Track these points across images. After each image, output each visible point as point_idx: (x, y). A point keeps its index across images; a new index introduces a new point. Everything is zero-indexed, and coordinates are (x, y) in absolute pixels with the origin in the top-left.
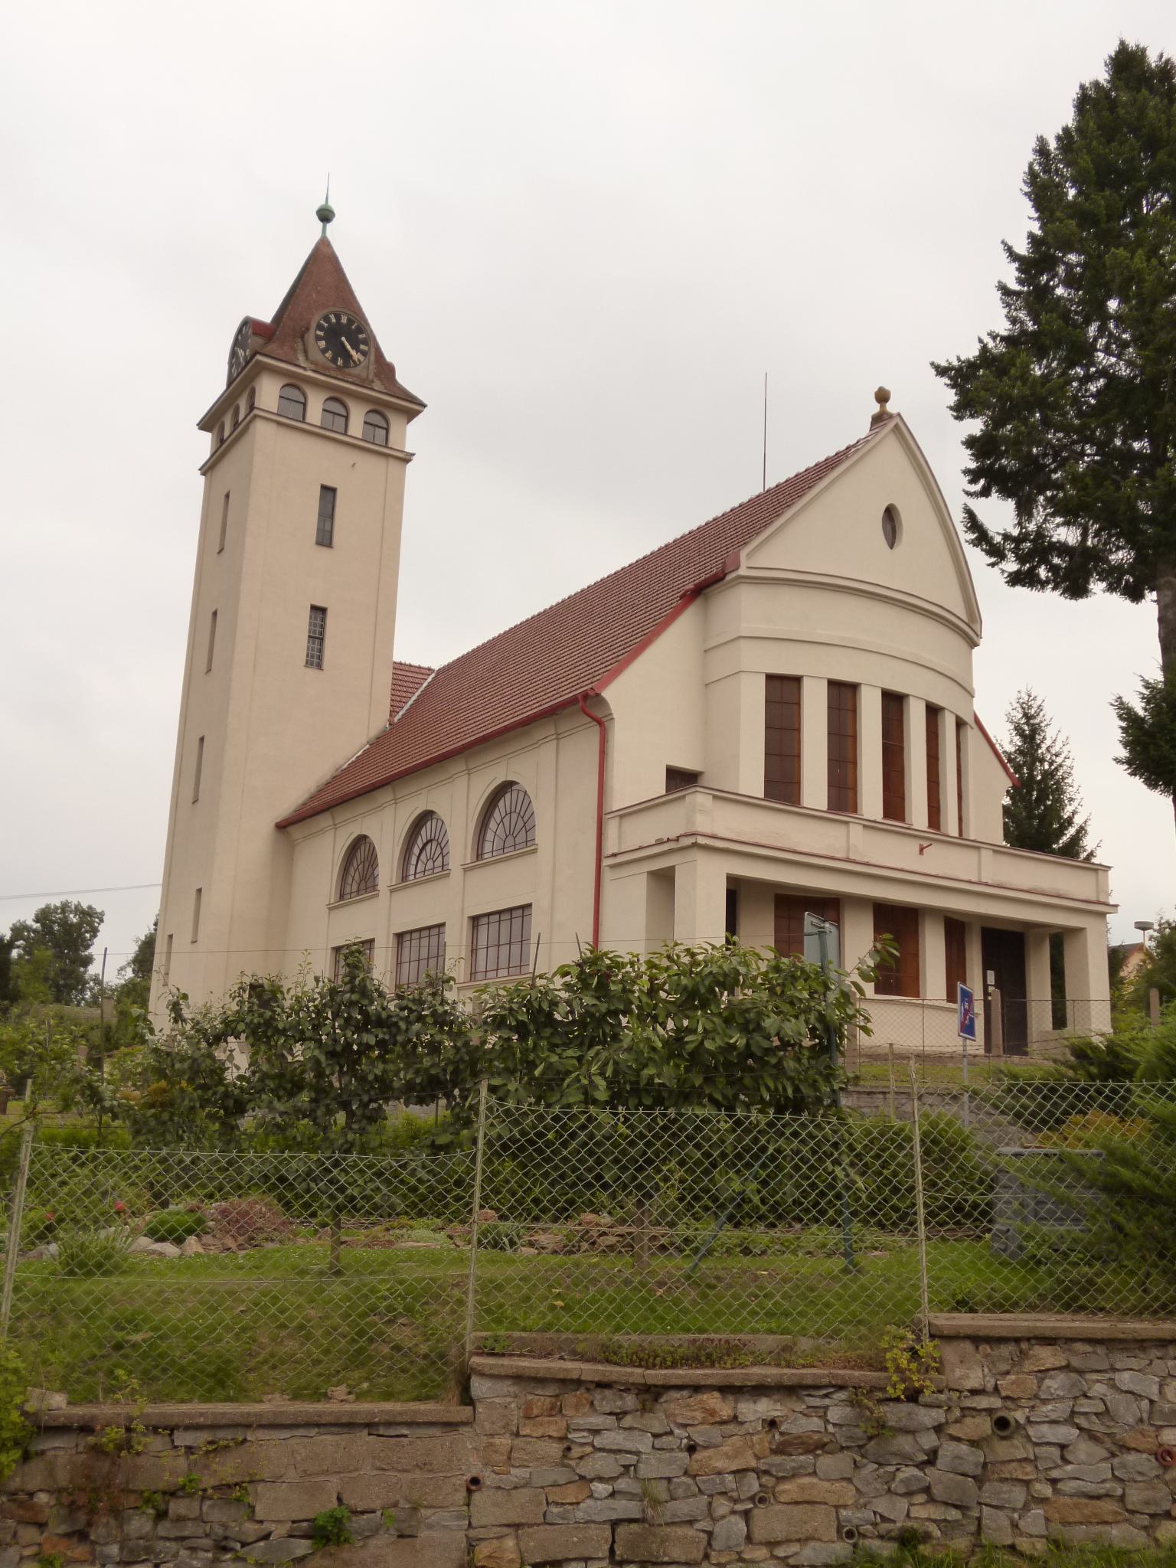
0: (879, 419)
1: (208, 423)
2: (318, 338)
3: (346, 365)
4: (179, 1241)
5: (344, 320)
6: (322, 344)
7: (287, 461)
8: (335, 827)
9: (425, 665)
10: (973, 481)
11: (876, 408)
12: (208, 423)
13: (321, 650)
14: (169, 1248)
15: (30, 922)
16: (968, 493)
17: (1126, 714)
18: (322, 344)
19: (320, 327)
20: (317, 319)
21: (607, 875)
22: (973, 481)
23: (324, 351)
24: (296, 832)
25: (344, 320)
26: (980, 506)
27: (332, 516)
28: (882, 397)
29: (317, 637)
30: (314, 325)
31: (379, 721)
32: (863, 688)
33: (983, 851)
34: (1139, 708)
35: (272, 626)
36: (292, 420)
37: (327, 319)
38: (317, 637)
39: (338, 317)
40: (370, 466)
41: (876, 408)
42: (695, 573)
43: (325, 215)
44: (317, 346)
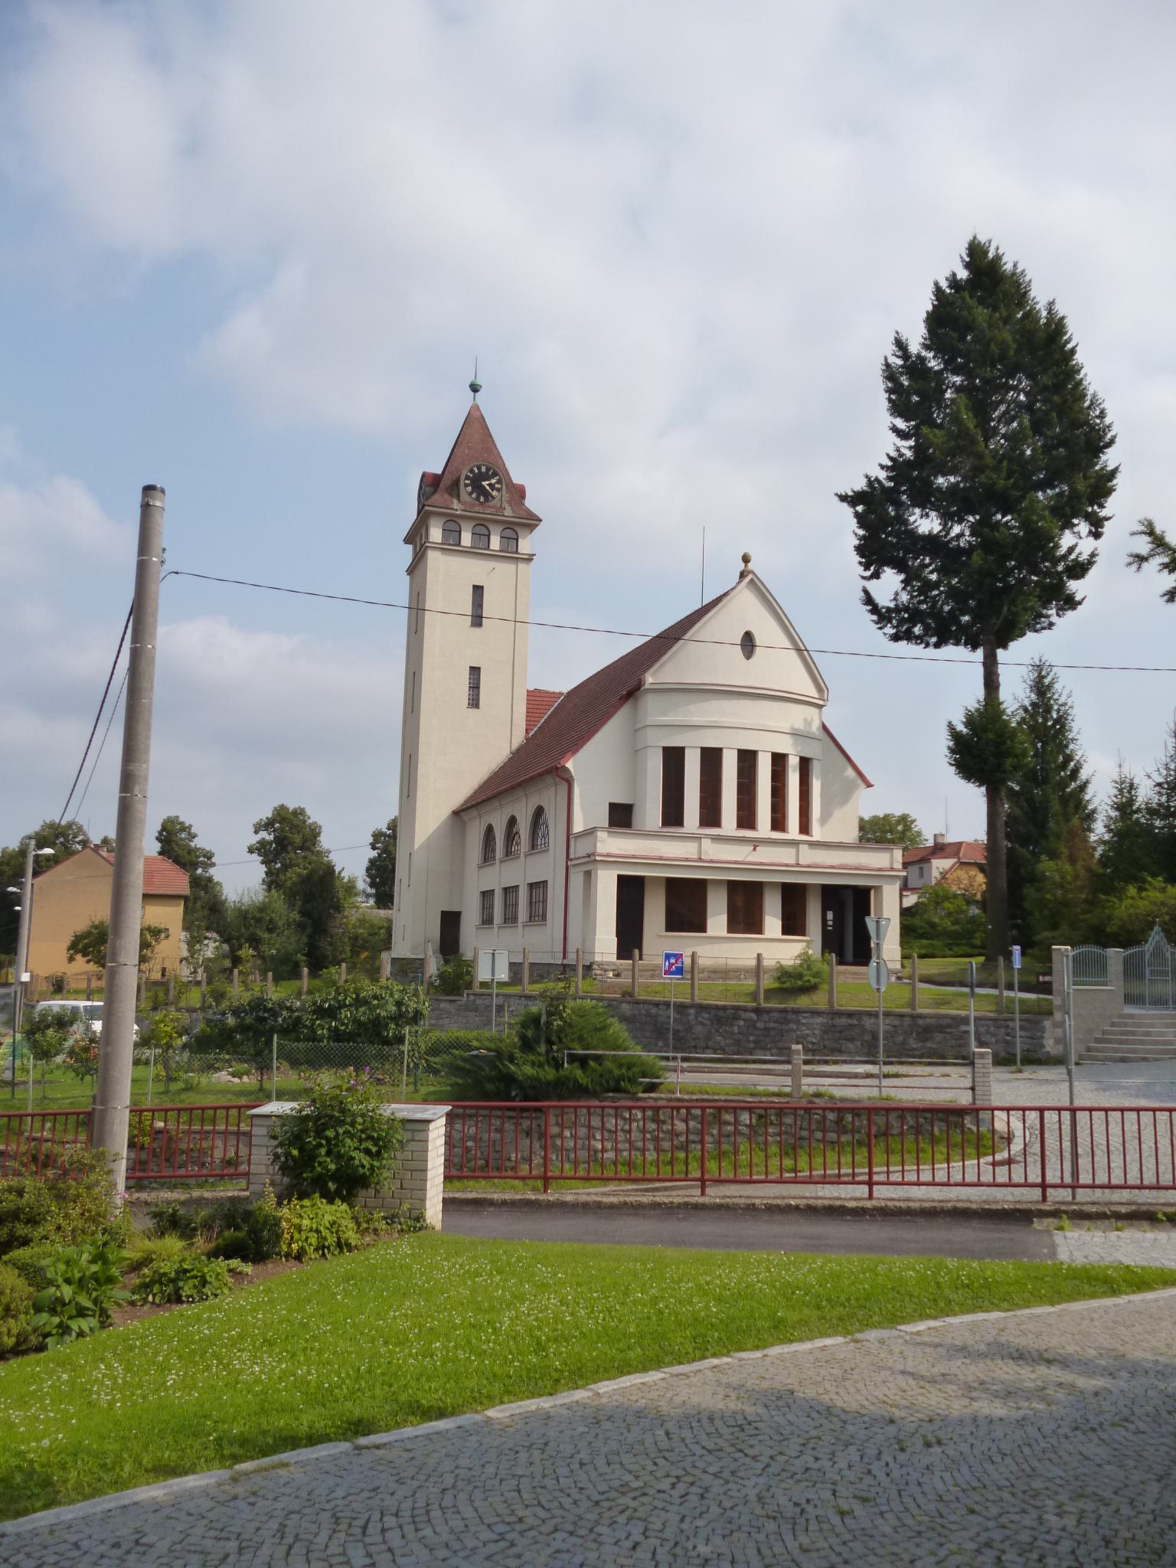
0: (742, 575)
1: (409, 539)
2: (466, 485)
3: (487, 500)
4: (240, 1078)
5: (484, 469)
6: (469, 489)
7: (450, 575)
8: (501, 806)
9: (557, 690)
10: (867, 568)
11: (741, 566)
12: (409, 539)
13: (478, 695)
14: (236, 1080)
15: (384, 830)
16: (863, 578)
17: (955, 735)
18: (469, 489)
19: (467, 478)
20: (465, 472)
21: (572, 870)
22: (867, 568)
23: (470, 494)
24: (466, 816)
25: (484, 469)
26: (873, 586)
27: (481, 606)
28: (746, 559)
29: (475, 687)
30: (463, 477)
31: (519, 738)
32: (725, 752)
33: (801, 846)
34: (961, 728)
35: (444, 683)
36: (451, 545)
37: (472, 471)
38: (475, 687)
39: (479, 468)
40: (505, 568)
41: (741, 566)
42: (620, 686)
43: (475, 388)
44: (465, 491)
